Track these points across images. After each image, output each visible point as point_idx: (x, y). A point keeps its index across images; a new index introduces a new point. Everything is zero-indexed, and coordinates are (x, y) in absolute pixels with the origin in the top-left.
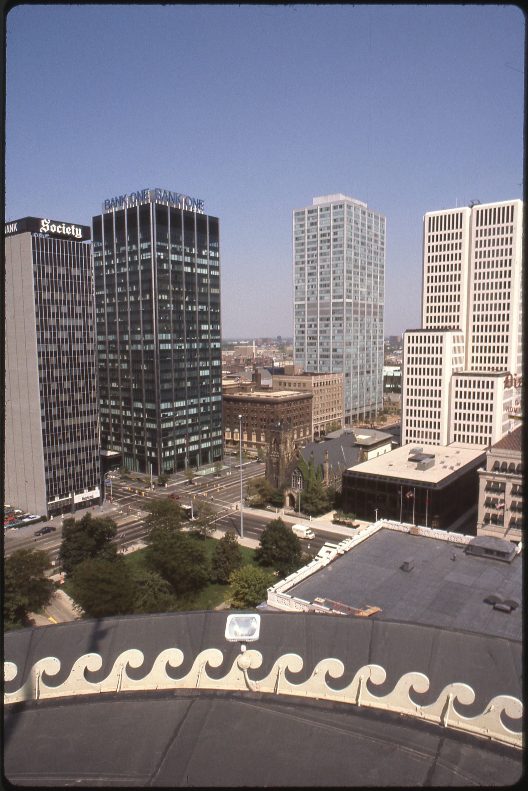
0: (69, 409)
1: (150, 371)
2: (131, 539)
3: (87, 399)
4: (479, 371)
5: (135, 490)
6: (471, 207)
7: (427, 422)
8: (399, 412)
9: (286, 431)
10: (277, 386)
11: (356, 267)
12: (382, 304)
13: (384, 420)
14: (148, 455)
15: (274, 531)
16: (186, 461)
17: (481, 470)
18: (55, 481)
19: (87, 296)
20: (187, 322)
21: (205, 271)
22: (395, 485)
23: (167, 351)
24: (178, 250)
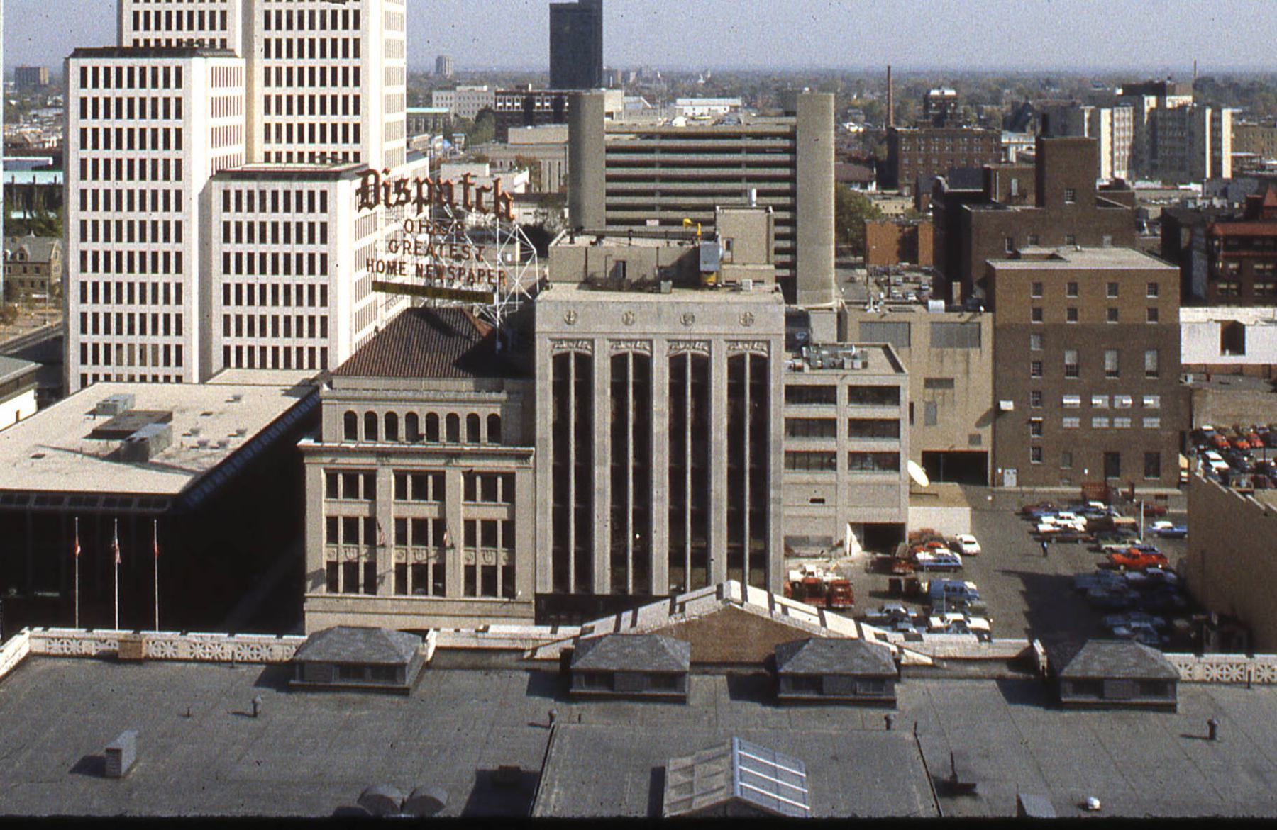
4: (284, 166)
8: (60, 297)
17: (305, 442)
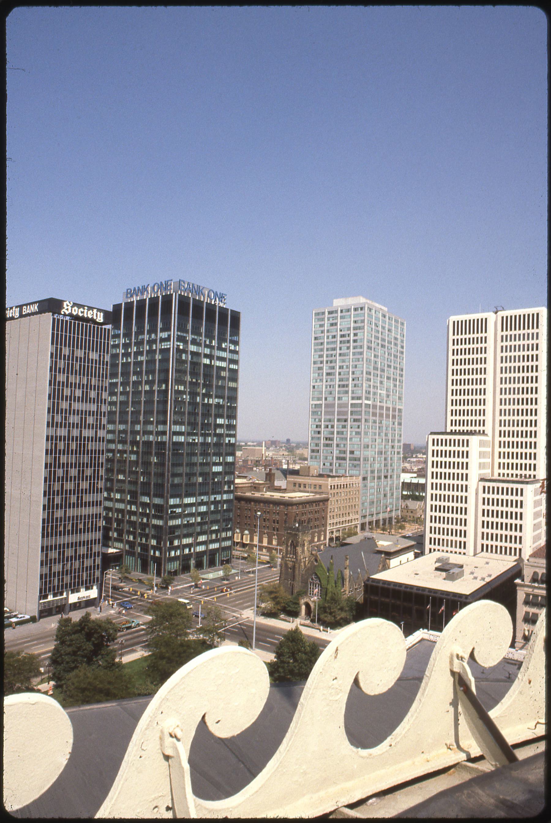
0: (73, 499)
1: (161, 464)
2: (129, 647)
3: (93, 489)
5: (137, 592)
6: (496, 313)
7: (452, 530)
8: (421, 521)
9: (304, 533)
10: (291, 487)
11: (376, 368)
12: (400, 407)
13: (403, 527)
14: (152, 554)
15: (291, 642)
16: (193, 562)
17: (518, 581)
18: (50, 577)
19: (102, 381)
20: (203, 414)
21: (223, 364)
22: (422, 596)
23: (180, 444)
24: (198, 341)
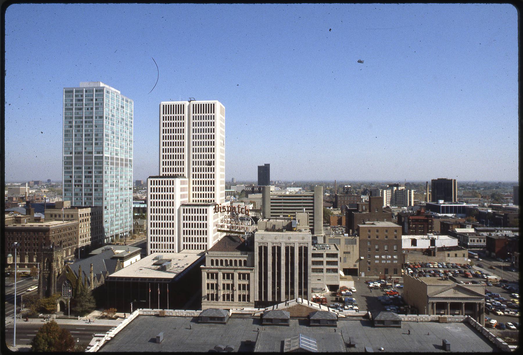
4: (197, 203)
6: (190, 102)
17: (202, 266)
